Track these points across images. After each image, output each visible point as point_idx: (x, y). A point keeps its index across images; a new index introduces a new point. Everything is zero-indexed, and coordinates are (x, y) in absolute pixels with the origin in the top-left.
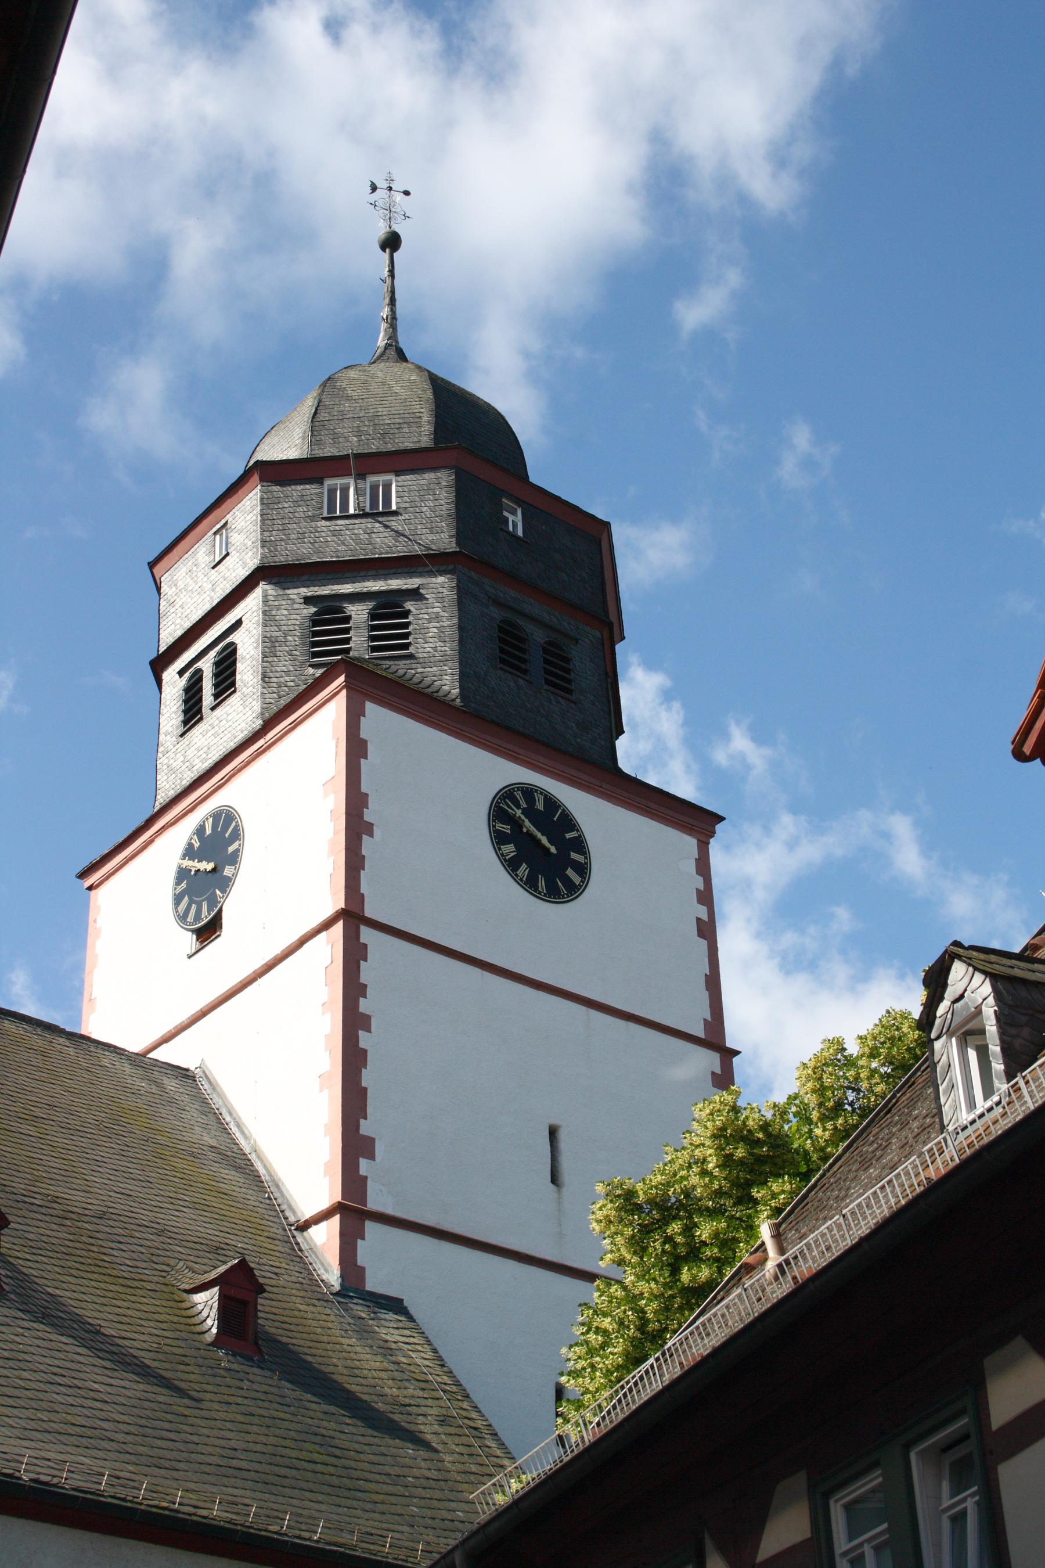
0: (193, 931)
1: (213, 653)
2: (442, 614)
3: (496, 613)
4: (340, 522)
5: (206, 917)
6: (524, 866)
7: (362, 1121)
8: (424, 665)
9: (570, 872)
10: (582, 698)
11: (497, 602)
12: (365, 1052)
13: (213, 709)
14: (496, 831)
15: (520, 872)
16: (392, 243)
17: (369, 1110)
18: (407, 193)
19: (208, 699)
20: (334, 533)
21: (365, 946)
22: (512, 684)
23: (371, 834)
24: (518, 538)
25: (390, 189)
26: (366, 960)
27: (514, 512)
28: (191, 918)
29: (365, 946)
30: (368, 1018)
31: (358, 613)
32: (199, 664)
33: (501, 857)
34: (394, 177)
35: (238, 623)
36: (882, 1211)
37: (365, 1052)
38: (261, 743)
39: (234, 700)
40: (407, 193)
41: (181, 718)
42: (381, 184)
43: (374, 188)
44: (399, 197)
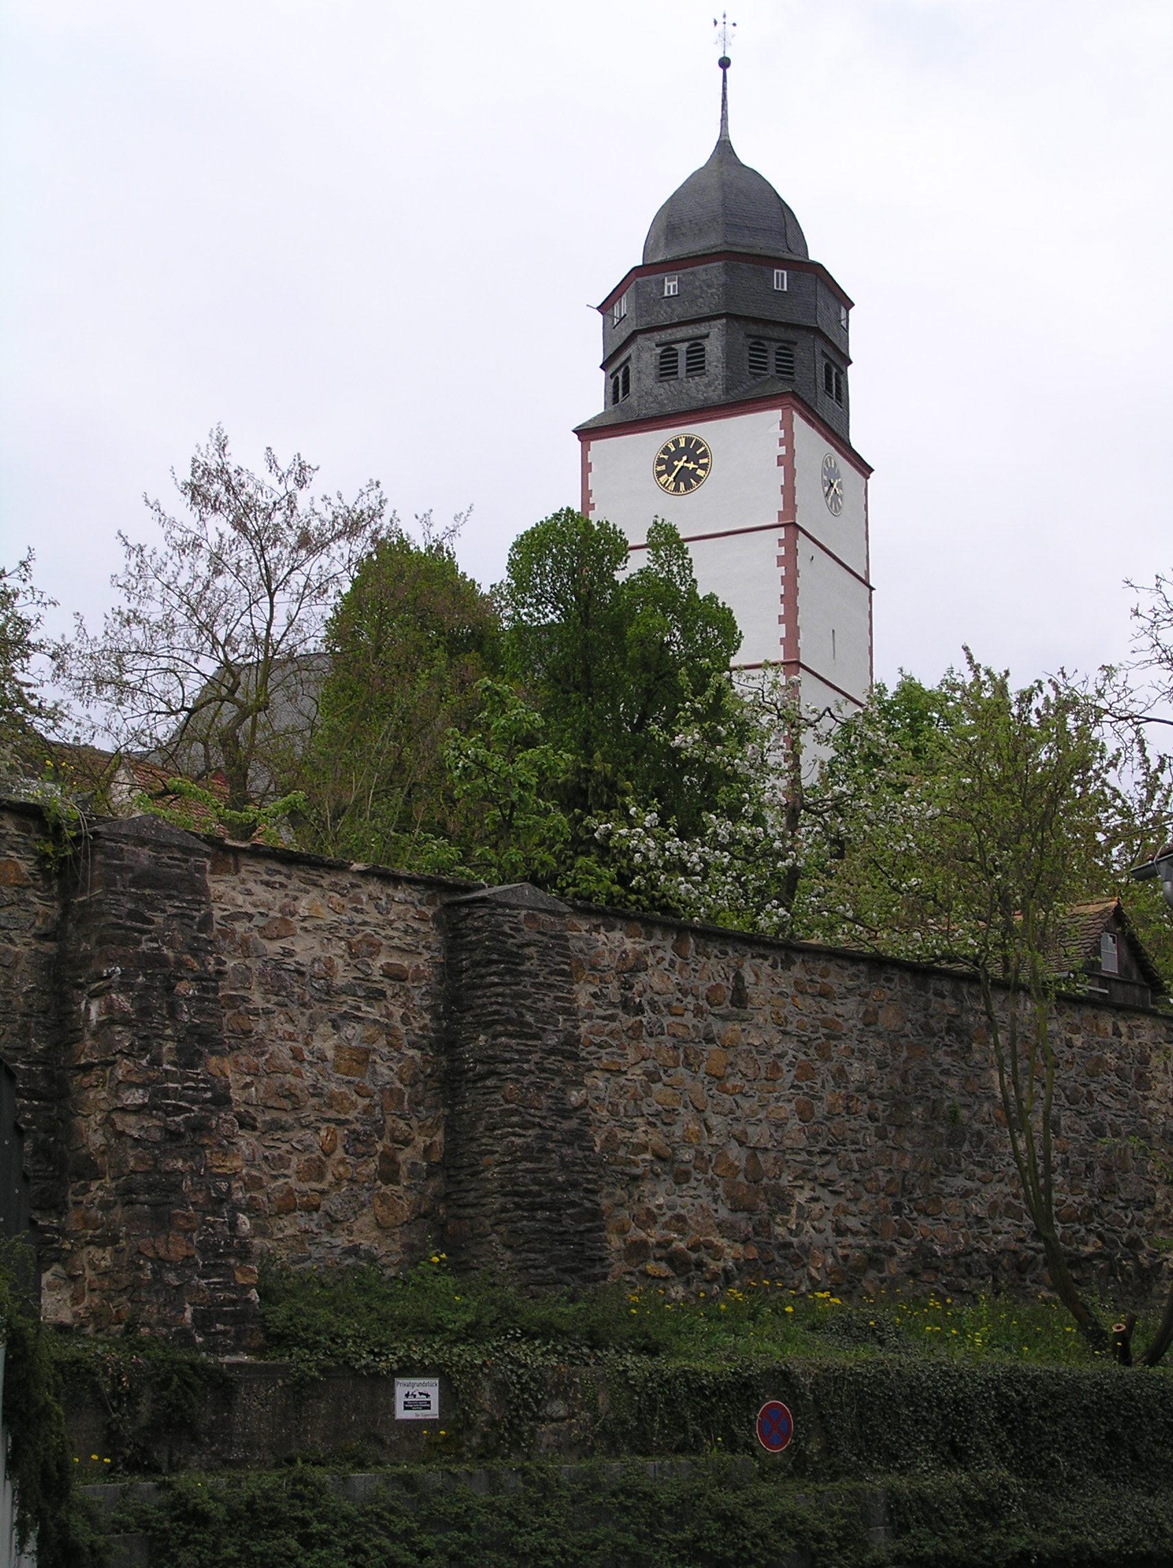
14: (702, 445)
16: (725, 63)
43: (716, 23)
44: (729, 27)
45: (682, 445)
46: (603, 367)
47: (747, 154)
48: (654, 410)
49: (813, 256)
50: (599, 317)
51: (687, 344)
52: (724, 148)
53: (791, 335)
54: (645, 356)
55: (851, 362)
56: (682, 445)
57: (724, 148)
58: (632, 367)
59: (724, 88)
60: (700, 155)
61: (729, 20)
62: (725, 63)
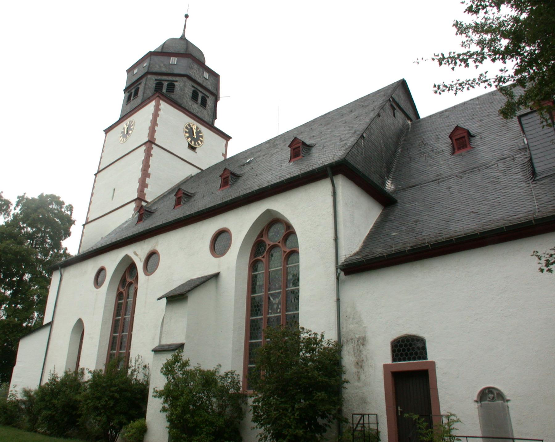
11: (193, 87)
16: (187, 16)
62: (187, 16)
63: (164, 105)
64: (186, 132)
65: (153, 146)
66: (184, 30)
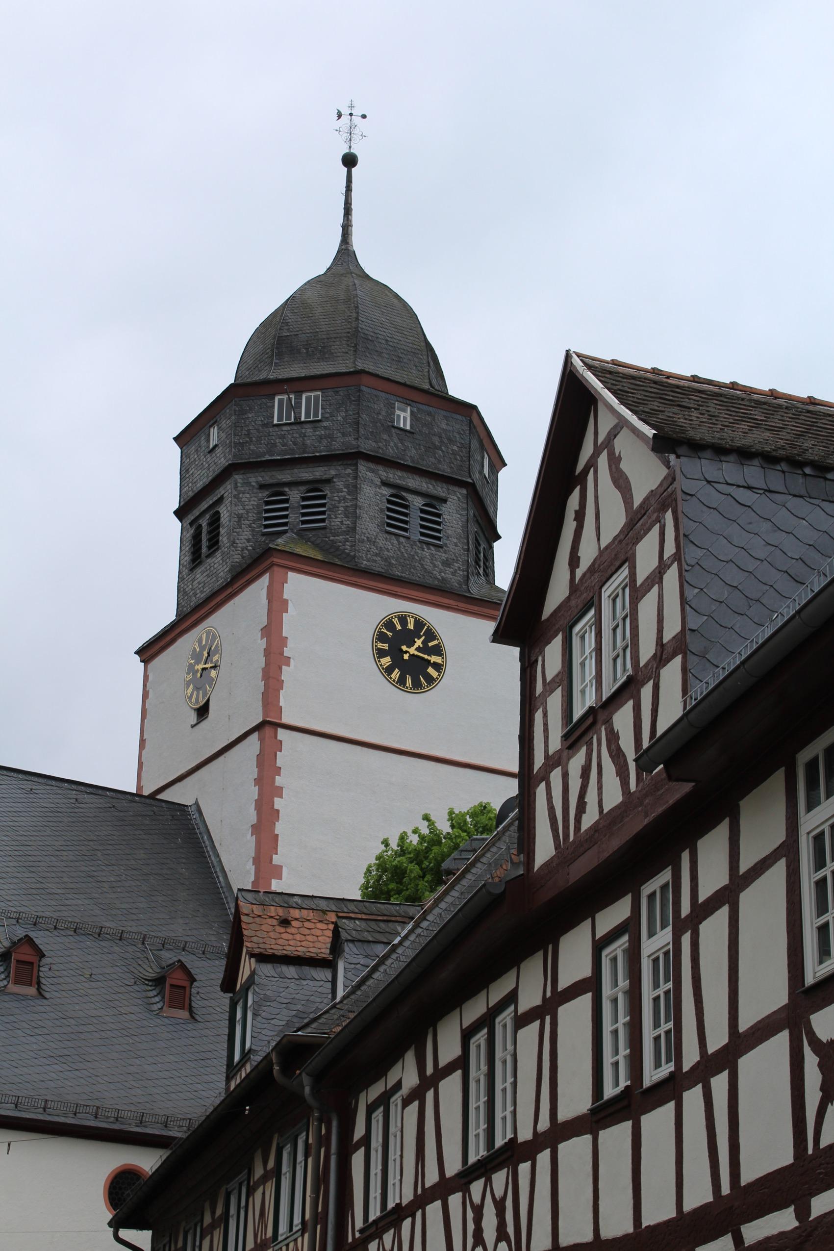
0: (195, 709)
1: (207, 516)
2: (347, 497)
3: (386, 492)
4: (285, 428)
5: (202, 702)
6: (397, 670)
7: (274, 856)
8: (335, 535)
9: (431, 670)
10: (448, 542)
11: (385, 484)
12: (278, 811)
13: (208, 556)
14: (378, 650)
15: (393, 676)
16: (350, 161)
17: (279, 849)
18: (364, 117)
19: (204, 550)
20: (282, 437)
21: (281, 742)
22: (395, 542)
23: (288, 665)
24: (406, 431)
25: (351, 115)
26: (281, 751)
27: (405, 411)
28: (193, 700)
29: (281, 742)
30: (281, 789)
31: (295, 495)
32: (200, 521)
33: (379, 666)
34: (354, 104)
35: (221, 500)
36: (61, 1121)
37: (278, 811)
38: (229, 590)
39: (218, 554)
40: (364, 117)
41: (191, 557)
42: (345, 111)
43: (340, 116)
44: (357, 120)
45: (386, 646)
46: (180, 513)
47: (373, 262)
48: (378, 566)
49: (456, 388)
50: (177, 450)
51: (303, 488)
52: (345, 253)
53: (439, 490)
54: (239, 505)
55: (498, 537)
56: (386, 646)
57: (345, 253)
58: (224, 512)
59: (349, 189)
60: (319, 261)
61: (357, 112)
62: (350, 161)
63: (299, 586)
64: (381, 653)
65: (282, 734)
66: (346, 228)
